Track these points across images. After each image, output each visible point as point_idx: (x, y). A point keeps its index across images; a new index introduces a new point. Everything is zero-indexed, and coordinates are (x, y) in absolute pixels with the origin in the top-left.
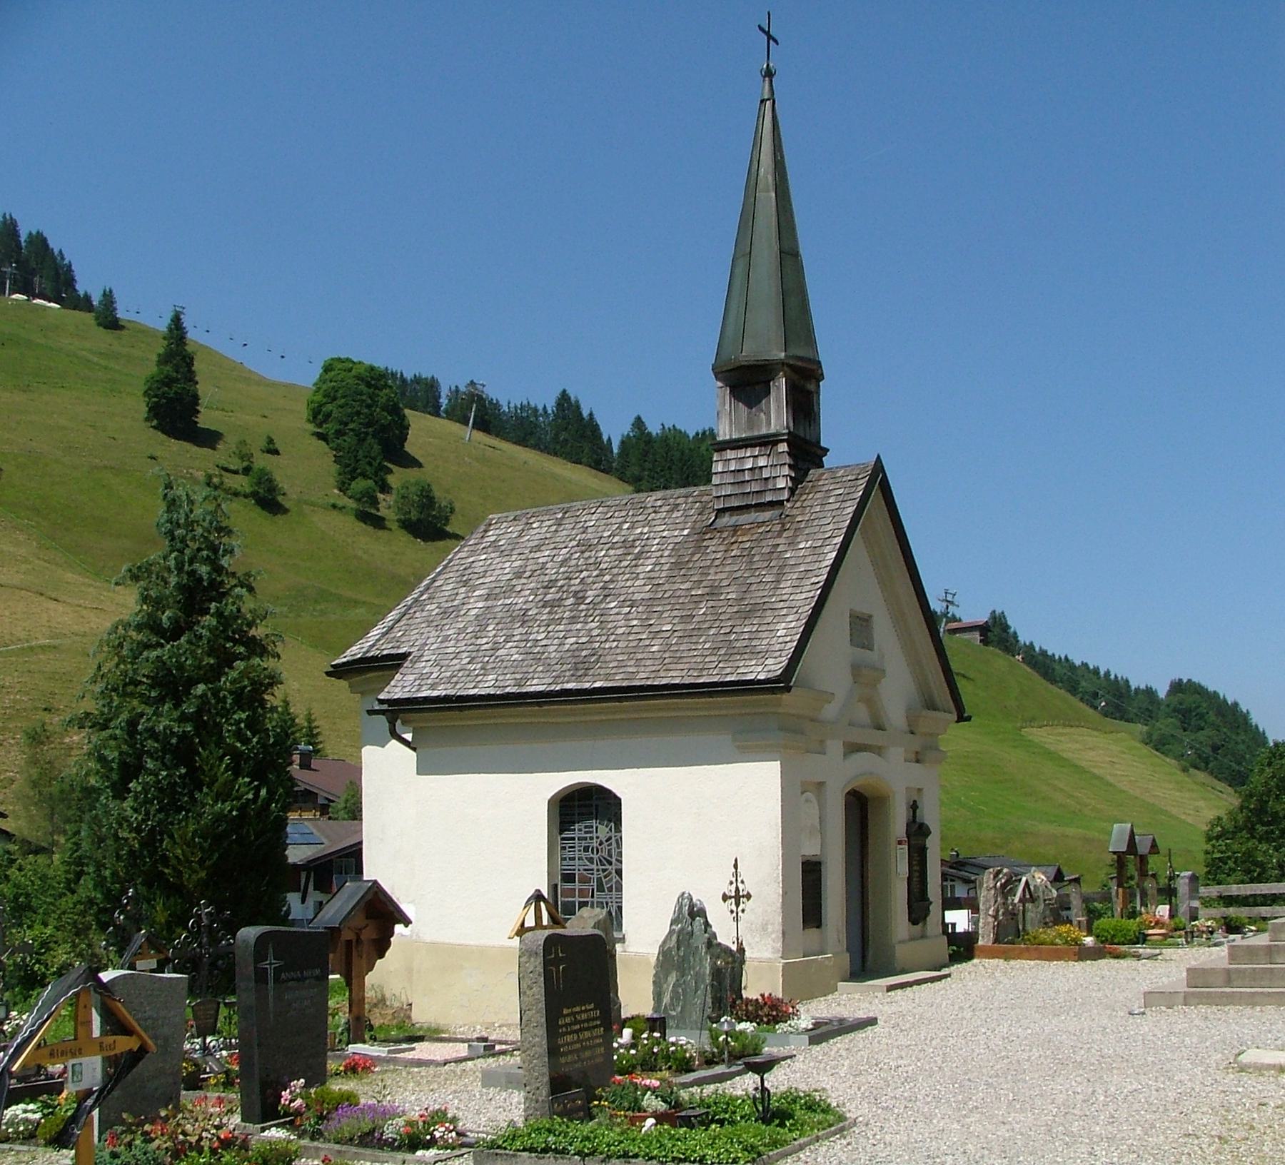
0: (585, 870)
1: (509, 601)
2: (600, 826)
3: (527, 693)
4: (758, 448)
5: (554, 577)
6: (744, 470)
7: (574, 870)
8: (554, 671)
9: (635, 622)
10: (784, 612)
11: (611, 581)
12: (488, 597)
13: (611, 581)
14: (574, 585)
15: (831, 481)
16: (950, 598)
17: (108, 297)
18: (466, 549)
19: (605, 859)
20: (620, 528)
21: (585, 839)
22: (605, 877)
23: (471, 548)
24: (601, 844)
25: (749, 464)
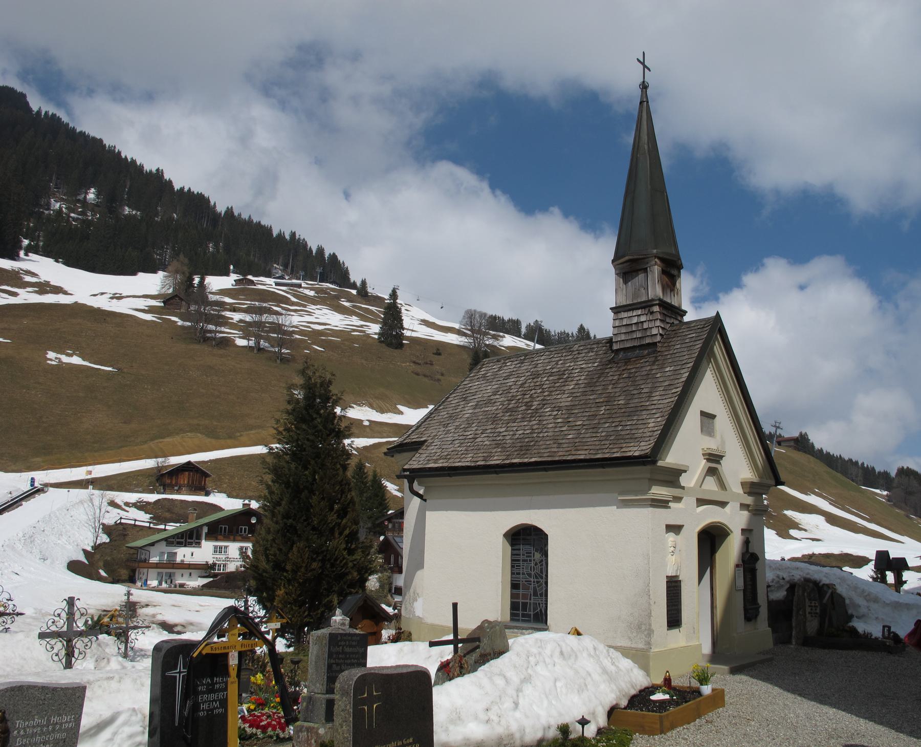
0: (526, 581)
1: (487, 409)
2: (536, 553)
3: (489, 465)
4: (640, 310)
5: (515, 394)
6: (632, 324)
7: (519, 581)
8: (507, 451)
9: (559, 420)
10: (654, 411)
11: (548, 395)
12: (476, 407)
13: (548, 395)
14: (526, 398)
15: (688, 329)
16: (777, 425)
17: (364, 283)
18: (468, 379)
19: (538, 574)
20: (557, 364)
21: (527, 561)
22: (539, 587)
23: (471, 378)
24: (536, 564)
25: (635, 320)
